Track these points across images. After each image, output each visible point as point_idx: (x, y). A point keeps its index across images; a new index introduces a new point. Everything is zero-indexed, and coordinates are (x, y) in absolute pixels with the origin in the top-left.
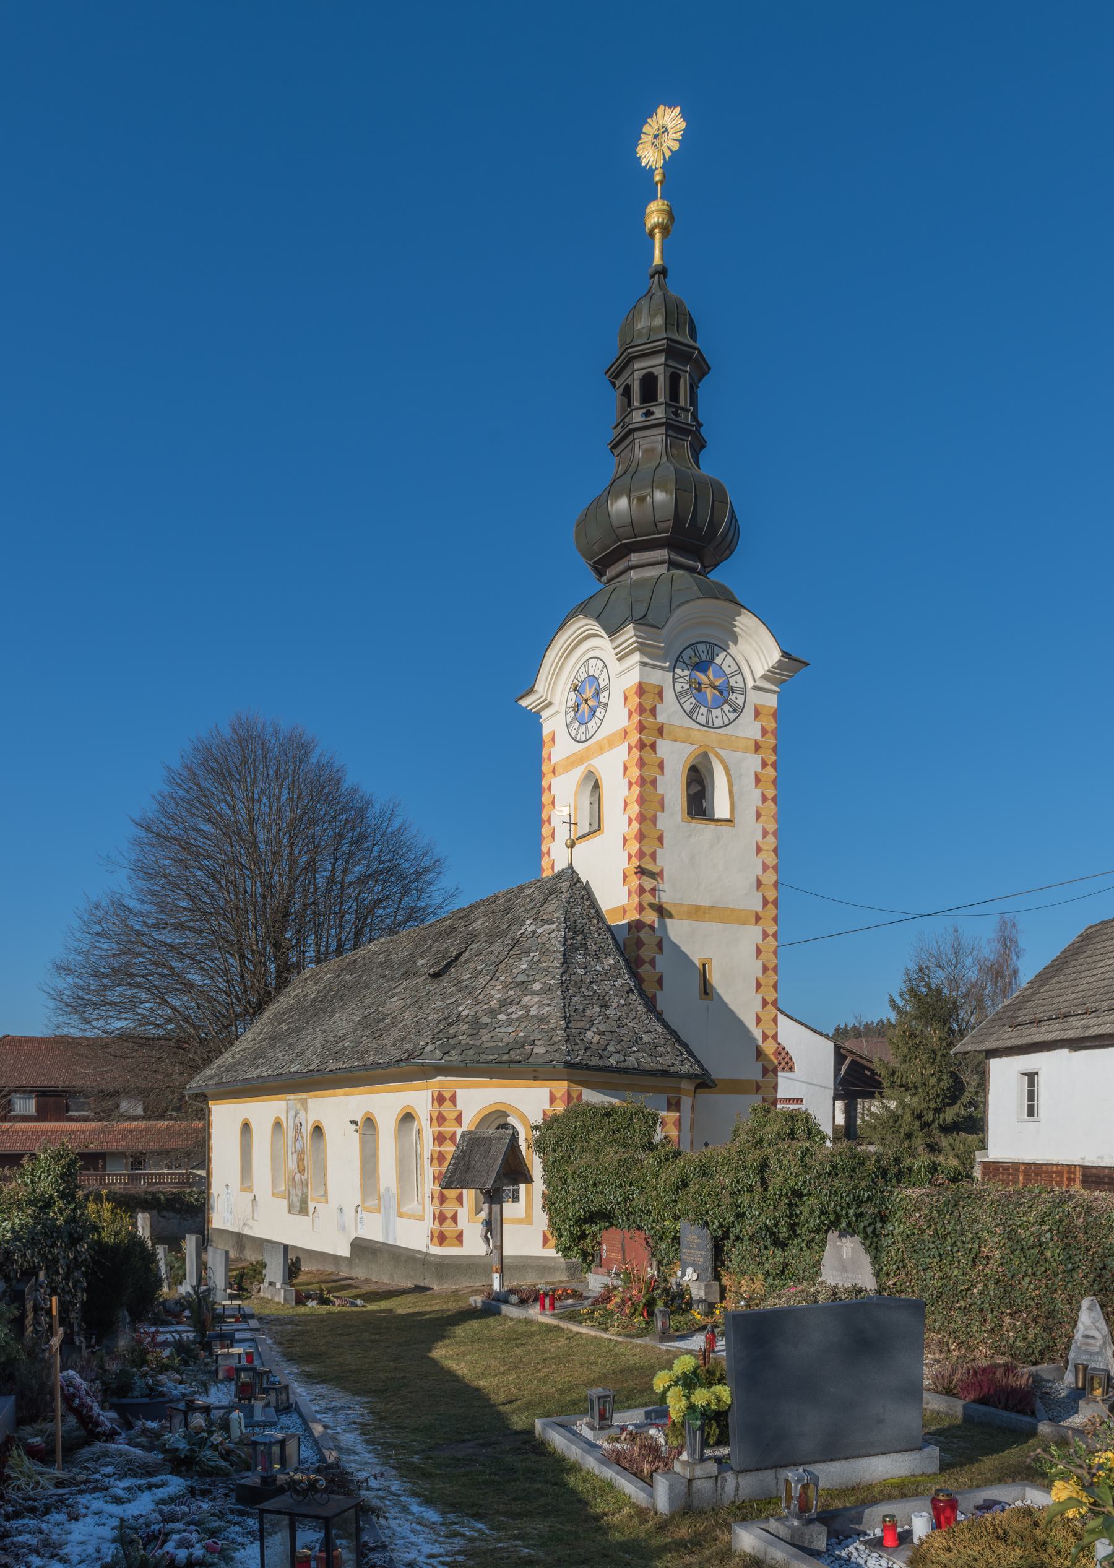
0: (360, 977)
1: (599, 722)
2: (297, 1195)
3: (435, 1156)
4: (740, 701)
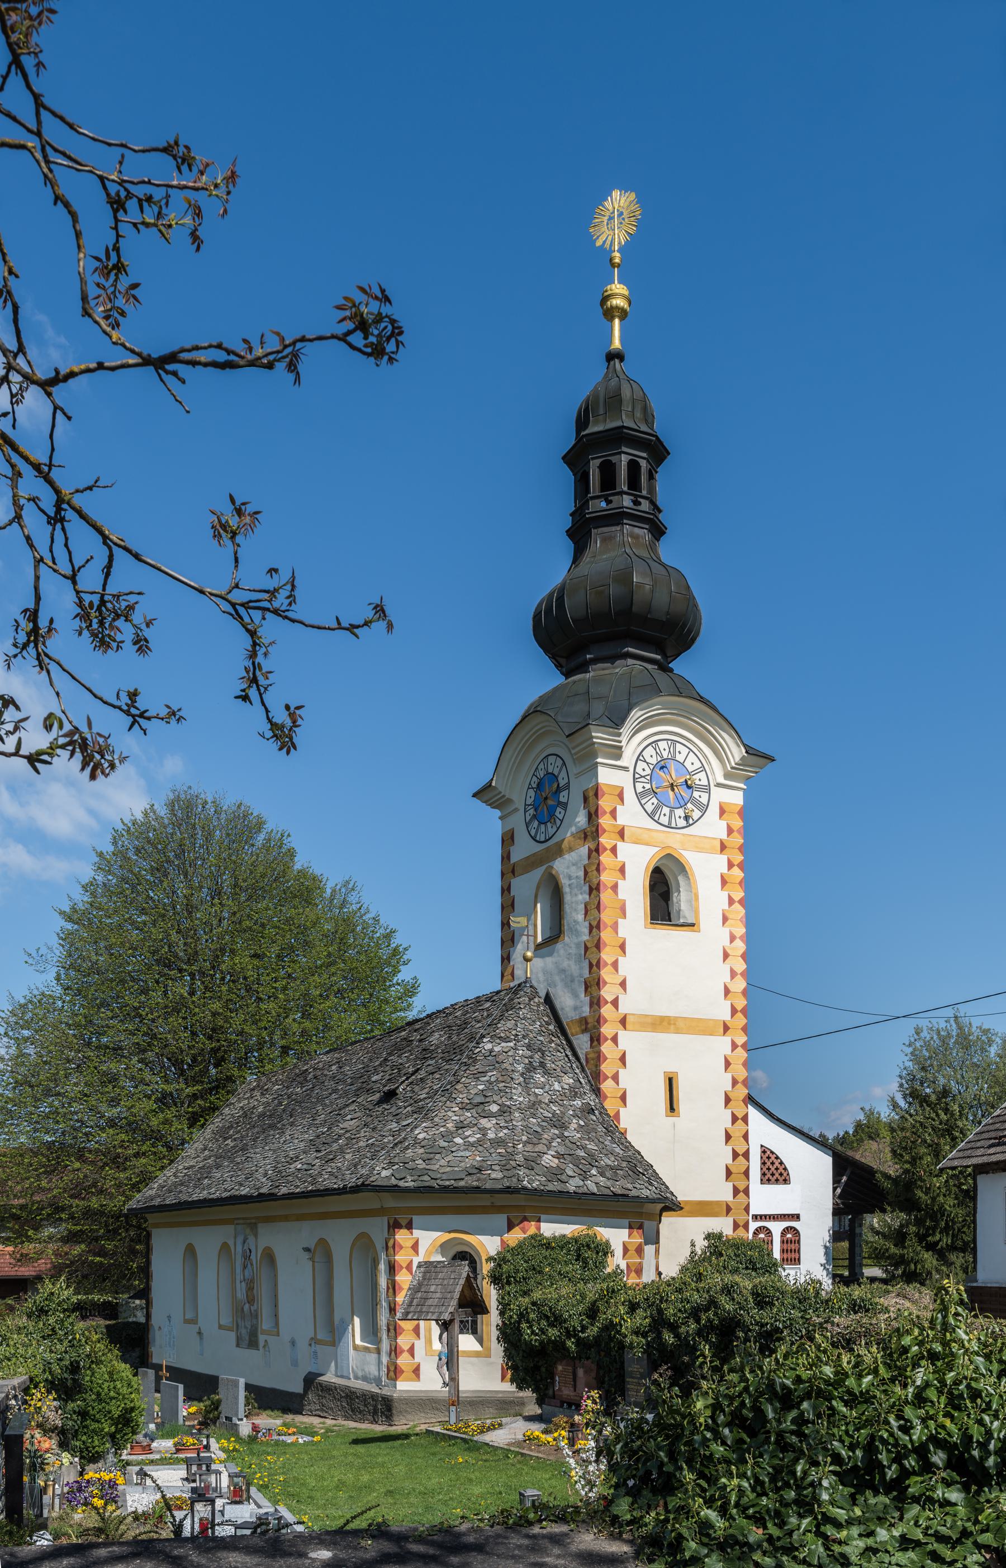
0: (312, 1089)
2: (246, 1327)
4: (704, 799)
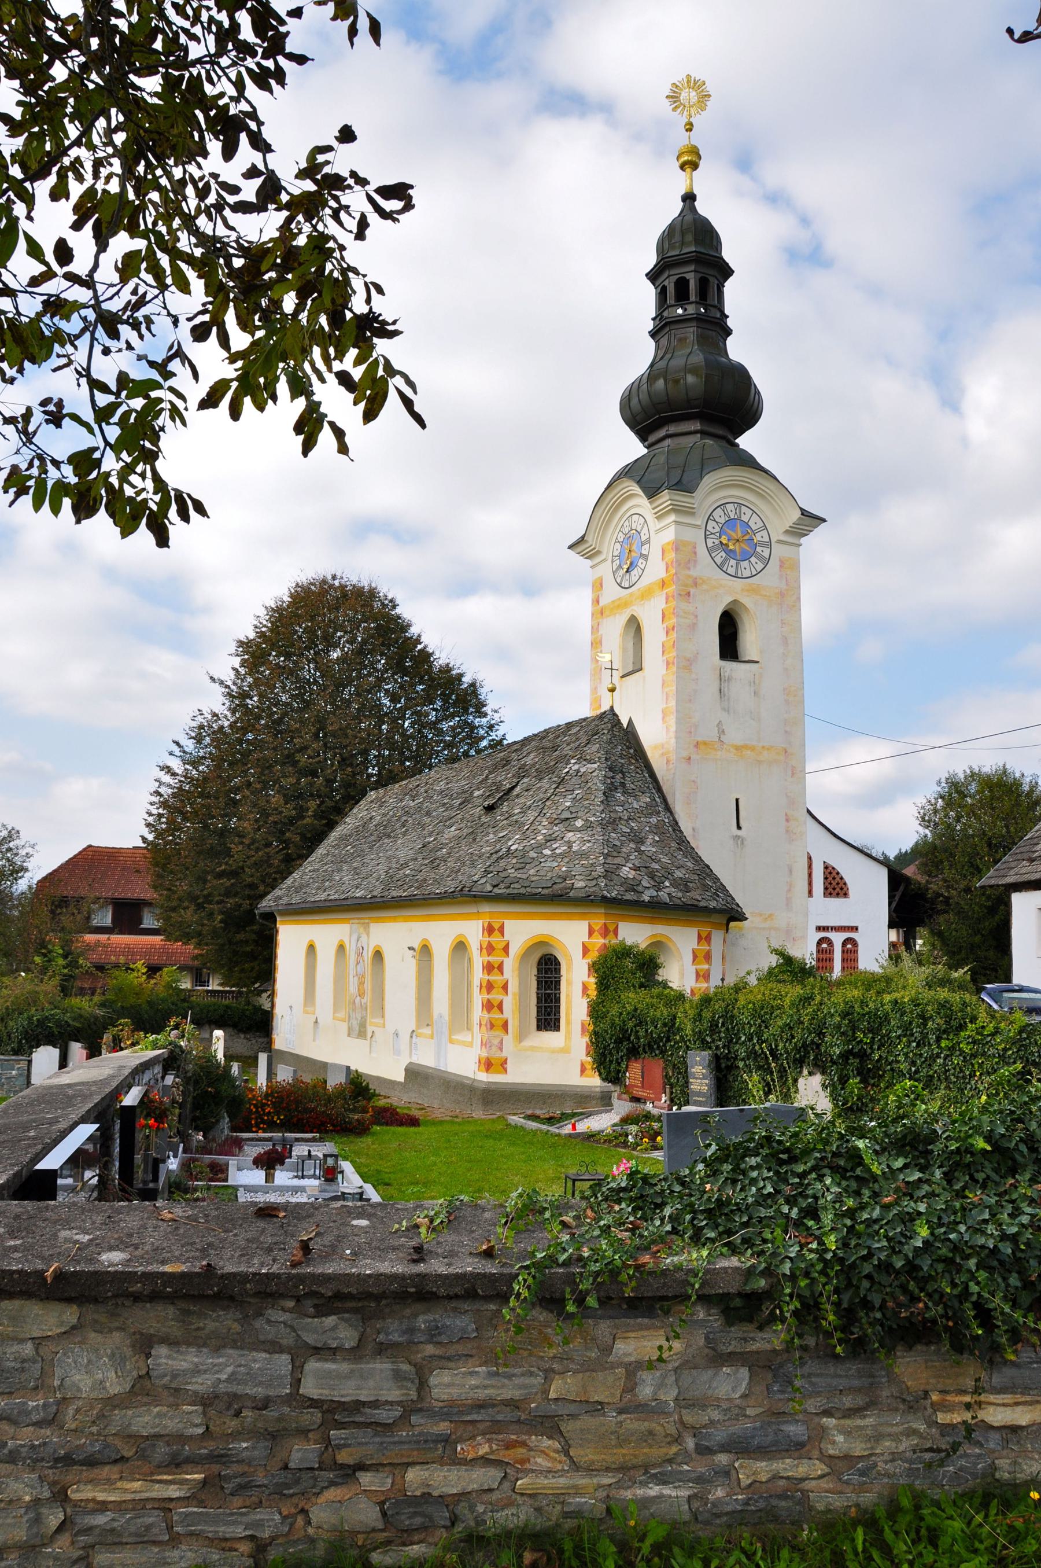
1: (640, 571)
3: (484, 984)
4: (766, 554)
